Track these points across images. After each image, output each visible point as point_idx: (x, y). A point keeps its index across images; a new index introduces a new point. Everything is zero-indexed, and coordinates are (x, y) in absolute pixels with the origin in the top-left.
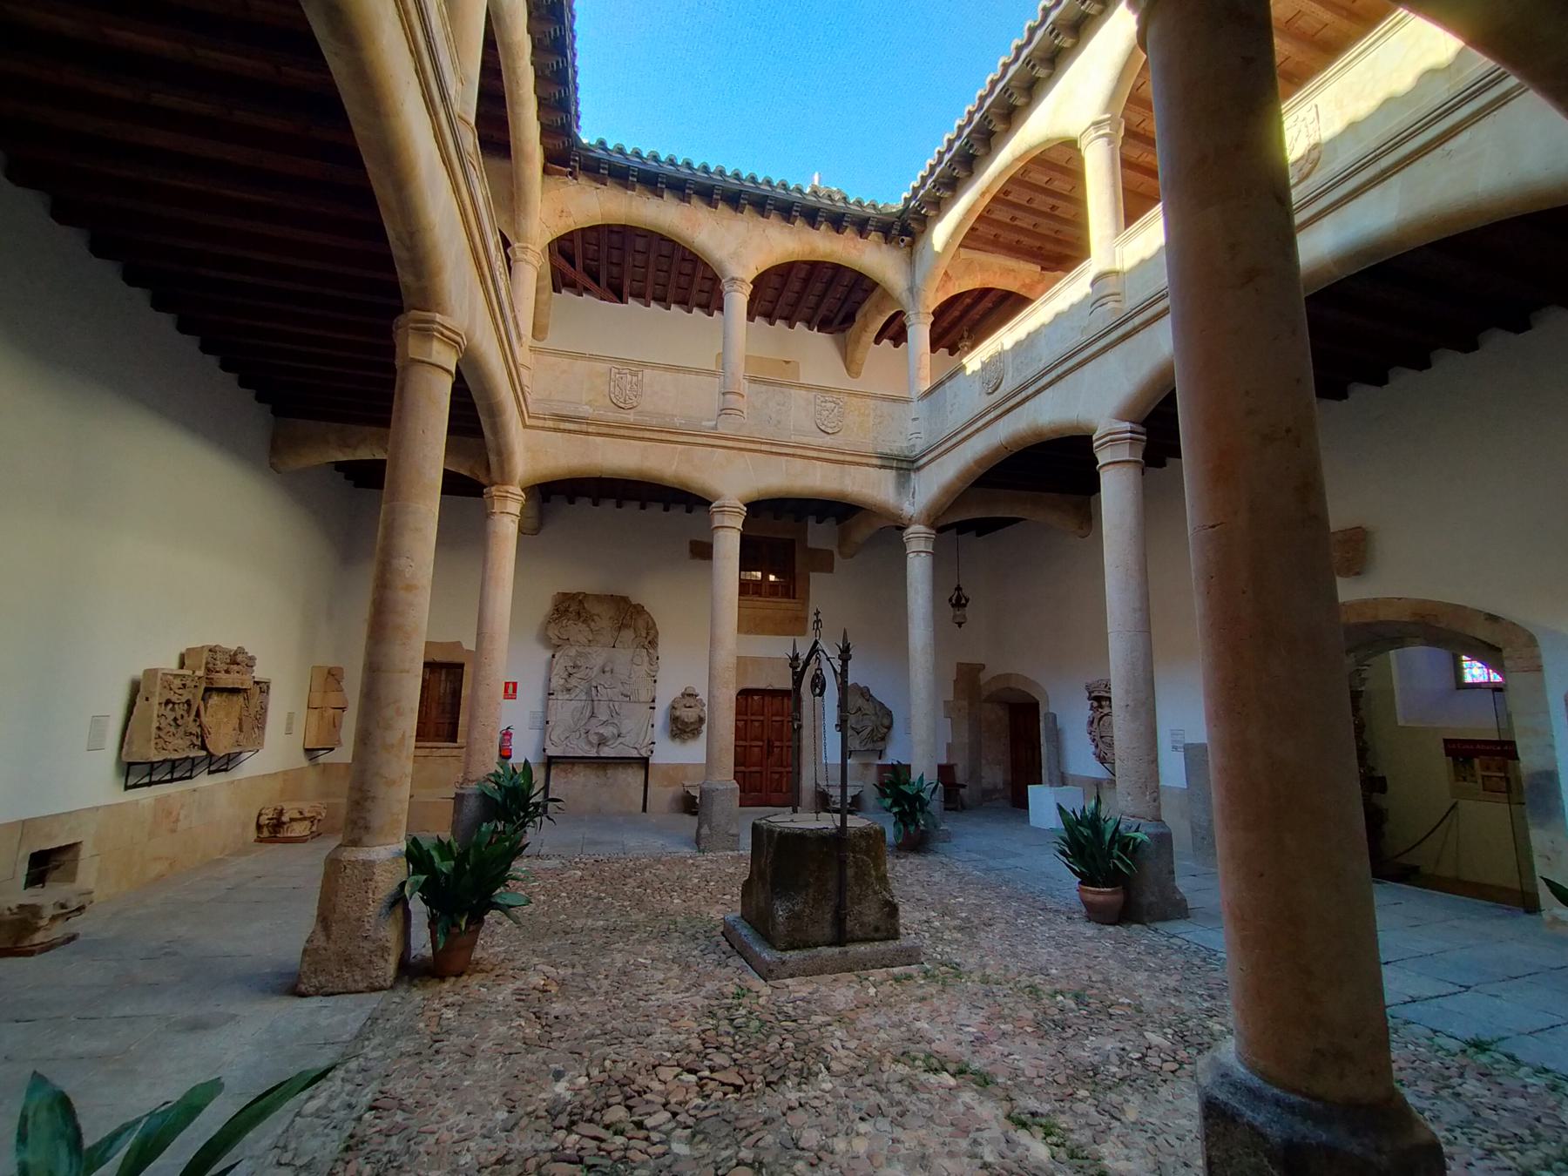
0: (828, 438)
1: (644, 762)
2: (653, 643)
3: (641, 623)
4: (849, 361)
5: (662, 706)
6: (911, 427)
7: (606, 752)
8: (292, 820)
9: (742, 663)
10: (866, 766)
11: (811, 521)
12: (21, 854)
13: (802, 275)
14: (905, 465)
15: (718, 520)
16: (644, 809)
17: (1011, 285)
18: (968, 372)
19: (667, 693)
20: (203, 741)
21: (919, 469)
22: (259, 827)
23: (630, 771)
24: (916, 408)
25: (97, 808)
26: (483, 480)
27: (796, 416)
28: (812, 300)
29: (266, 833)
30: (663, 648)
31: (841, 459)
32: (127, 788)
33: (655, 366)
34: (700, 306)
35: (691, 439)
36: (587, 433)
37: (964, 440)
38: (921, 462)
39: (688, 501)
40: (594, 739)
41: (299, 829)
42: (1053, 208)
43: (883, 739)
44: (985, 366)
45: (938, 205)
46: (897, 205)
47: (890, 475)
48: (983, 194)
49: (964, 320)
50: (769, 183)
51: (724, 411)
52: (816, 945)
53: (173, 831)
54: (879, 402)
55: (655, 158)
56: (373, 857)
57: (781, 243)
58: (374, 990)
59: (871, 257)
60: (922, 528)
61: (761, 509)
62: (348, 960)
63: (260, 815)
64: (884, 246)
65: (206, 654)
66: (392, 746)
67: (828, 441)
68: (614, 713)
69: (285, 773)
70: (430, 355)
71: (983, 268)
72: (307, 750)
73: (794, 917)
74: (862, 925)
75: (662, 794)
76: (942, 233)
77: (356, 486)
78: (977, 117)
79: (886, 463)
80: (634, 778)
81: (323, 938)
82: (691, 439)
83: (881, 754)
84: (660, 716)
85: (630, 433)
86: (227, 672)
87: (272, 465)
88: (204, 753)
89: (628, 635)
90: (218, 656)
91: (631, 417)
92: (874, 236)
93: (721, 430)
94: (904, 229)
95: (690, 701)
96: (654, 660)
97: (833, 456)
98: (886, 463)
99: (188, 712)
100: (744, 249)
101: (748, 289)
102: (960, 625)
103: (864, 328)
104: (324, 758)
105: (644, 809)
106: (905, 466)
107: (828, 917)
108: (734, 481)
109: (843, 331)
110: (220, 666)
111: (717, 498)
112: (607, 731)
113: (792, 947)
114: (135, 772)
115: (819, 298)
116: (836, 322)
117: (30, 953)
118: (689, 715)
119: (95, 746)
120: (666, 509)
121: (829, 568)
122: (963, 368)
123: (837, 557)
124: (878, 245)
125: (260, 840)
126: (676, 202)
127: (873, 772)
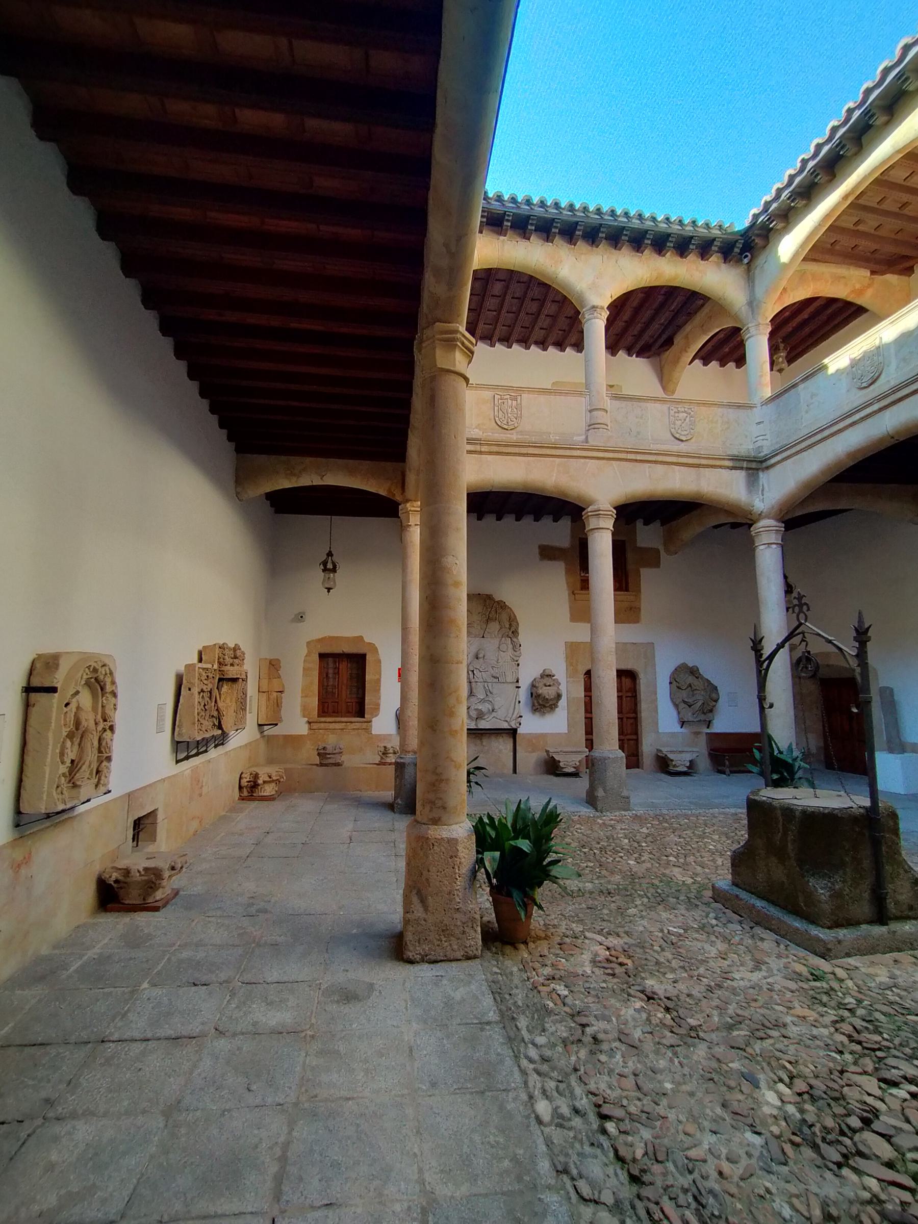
0: (683, 444)
1: (513, 733)
2: (515, 633)
3: (504, 616)
4: (664, 378)
5: (525, 683)
6: (756, 430)
7: (483, 725)
8: (264, 782)
9: (622, 648)
10: (697, 734)
11: (639, 524)
12: (129, 820)
13: (635, 304)
14: (754, 465)
15: (592, 523)
16: (515, 771)
17: (840, 292)
18: (831, 370)
19: (528, 674)
20: (220, 722)
21: (767, 468)
22: (240, 788)
23: (501, 740)
24: (758, 414)
25: (164, 780)
26: (398, 498)
27: (654, 425)
28: (639, 327)
29: (245, 793)
30: (522, 638)
31: (697, 462)
32: (177, 762)
33: (531, 390)
34: (537, 343)
35: (568, 453)
36: (481, 453)
37: (832, 435)
38: (773, 461)
39: (568, 510)
40: (474, 714)
41: (269, 790)
42: (904, 205)
43: (711, 711)
44: (854, 364)
45: (784, 215)
46: (741, 223)
47: (740, 475)
48: (846, 197)
49: (808, 327)
50: (626, 214)
51: (592, 426)
52: (858, 923)
53: (201, 795)
54: (725, 410)
55: (528, 202)
56: (455, 835)
57: (631, 271)
58: (468, 958)
59: (712, 277)
60: (772, 522)
61: (631, 513)
62: (445, 931)
63: (240, 778)
64: (723, 266)
65: (217, 650)
66: (456, 731)
67: (683, 447)
68: (488, 692)
69: (250, 743)
70: (454, 365)
71: (815, 277)
72: (260, 725)
73: (836, 895)
74: (897, 903)
75: (529, 759)
76: (789, 245)
77: (277, 512)
78: (857, 114)
79: (738, 464)
80: (503, 746)
81: (421, 909)
82: (568, 453)
83: (709, 724)
84: (523, 694)
85: (516, 450)
86: (232, 665)
87: (237, 494)
88: (220, 732)
89: (494, 626)
90: (226, 652)
91: (514, 437)
92: (715, 258)
93: (592, 442)
94: (745, 248)
95: (548, 681)
96: (516, 647)
97: (690, 461)
98: (738, 464)
99: (210, 698)
100: (598, 280)
101: (605, 314)
102: (329, 589)
103: (685, 349)
104: (270, 731)
105: (515, 771)
106: (754, 466)
107: (866, 895)
108: (604, 488)
109: (659, 355)
110: (228, 660)
111: (591, 503)
112: (485, 707)
113: (837, 924)
114: (184, 749)
115: (651, 324)
116: (653, 349)
117: (156, 909)
118: (547, 692)
119: (160, 731)
120: (499, 518)
121: (657, 564)
122: (825, 367)
123: (662, 552)
124: (718, 264)
125: (242, 799)
126: (541, 242)
127: (703, 740)
